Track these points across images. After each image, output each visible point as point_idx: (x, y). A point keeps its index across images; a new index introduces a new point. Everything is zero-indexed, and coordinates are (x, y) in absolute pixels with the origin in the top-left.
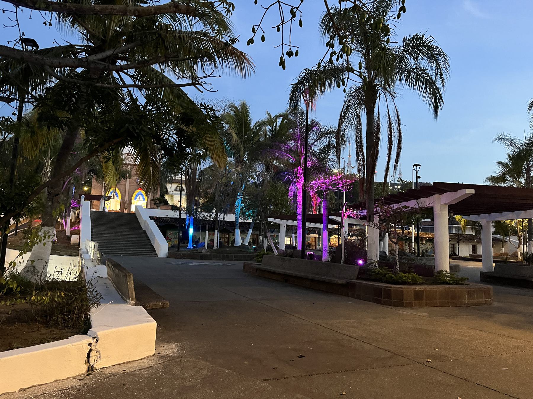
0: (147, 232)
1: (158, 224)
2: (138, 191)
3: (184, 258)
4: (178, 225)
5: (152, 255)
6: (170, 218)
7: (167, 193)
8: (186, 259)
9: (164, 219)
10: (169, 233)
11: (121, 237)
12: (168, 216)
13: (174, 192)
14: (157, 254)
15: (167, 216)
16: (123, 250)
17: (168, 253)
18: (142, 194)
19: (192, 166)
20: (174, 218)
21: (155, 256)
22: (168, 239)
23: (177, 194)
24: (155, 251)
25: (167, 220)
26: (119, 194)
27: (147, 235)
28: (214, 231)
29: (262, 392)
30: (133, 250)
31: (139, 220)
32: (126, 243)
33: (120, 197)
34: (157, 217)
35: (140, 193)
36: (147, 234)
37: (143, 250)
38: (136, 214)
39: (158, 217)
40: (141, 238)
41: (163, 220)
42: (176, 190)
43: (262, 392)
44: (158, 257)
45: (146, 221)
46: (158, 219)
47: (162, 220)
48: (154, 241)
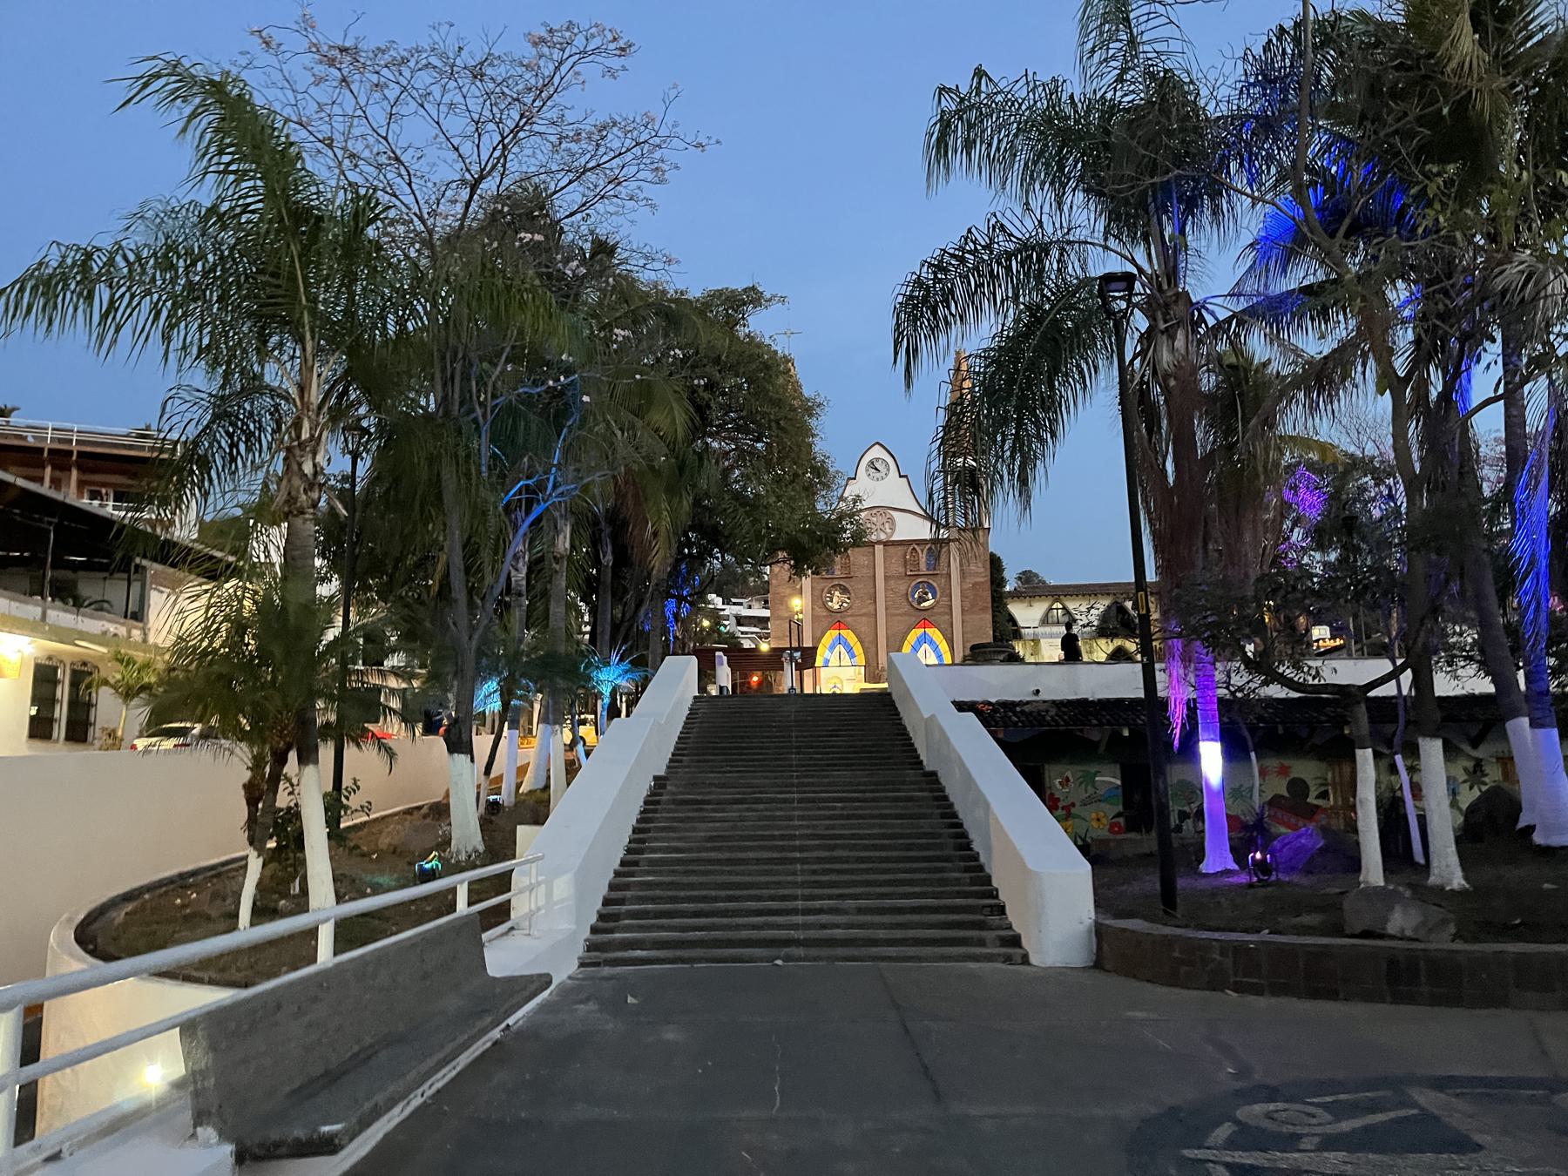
0: (943, 781)
1: (1001, 736)
2: (916, 633)
3: (1239, 988)
4: (1095, 736)
5: (982, 943)
6: (1054, 702)
7: (1017, 634)
8: (1257, 990)
9: (1027, 708)
10: (1055, 775)
11: (802, 818)
12: (1043, 696)
13: (1041, 630)
14: (1015, 941)
15: (1038, 691)
16: (795, 912)
17: (1099, 931)
18: (931, 642)
19: (1166, 358)
20: (1070, 703)
21: (1008, 959)
22: (1057, 808)
23: (1051, 636)
24: (1002, 910)
25: (1039, 712)
26: (858, 649)
27: (946, 798)
28: (1353, 760)
29: (477, 75)
30: (860, 911)
31: (906, 721)
32: (819, 860)
33: (861, 659)
34: (990, 703)
35: (924, 639)
36: (942, 790)
37: (914, 910)
38: (894, 697)
39: (993, 700)
40: (911, 817)
41: (1022, 712)
42: (1045, 621)
43: (477, 75)
44: (1025, 960)
45: (933, 716)
46: (995, 711)
47: (1015, 714)
48: (989, 849)
